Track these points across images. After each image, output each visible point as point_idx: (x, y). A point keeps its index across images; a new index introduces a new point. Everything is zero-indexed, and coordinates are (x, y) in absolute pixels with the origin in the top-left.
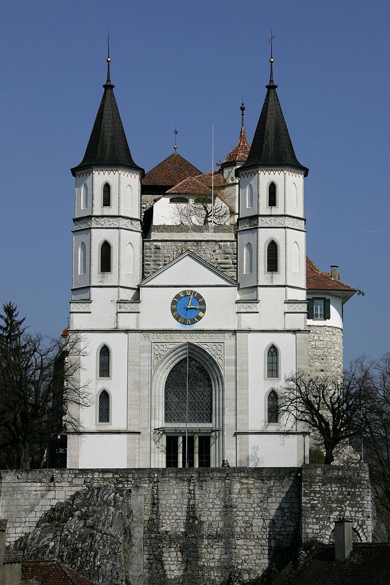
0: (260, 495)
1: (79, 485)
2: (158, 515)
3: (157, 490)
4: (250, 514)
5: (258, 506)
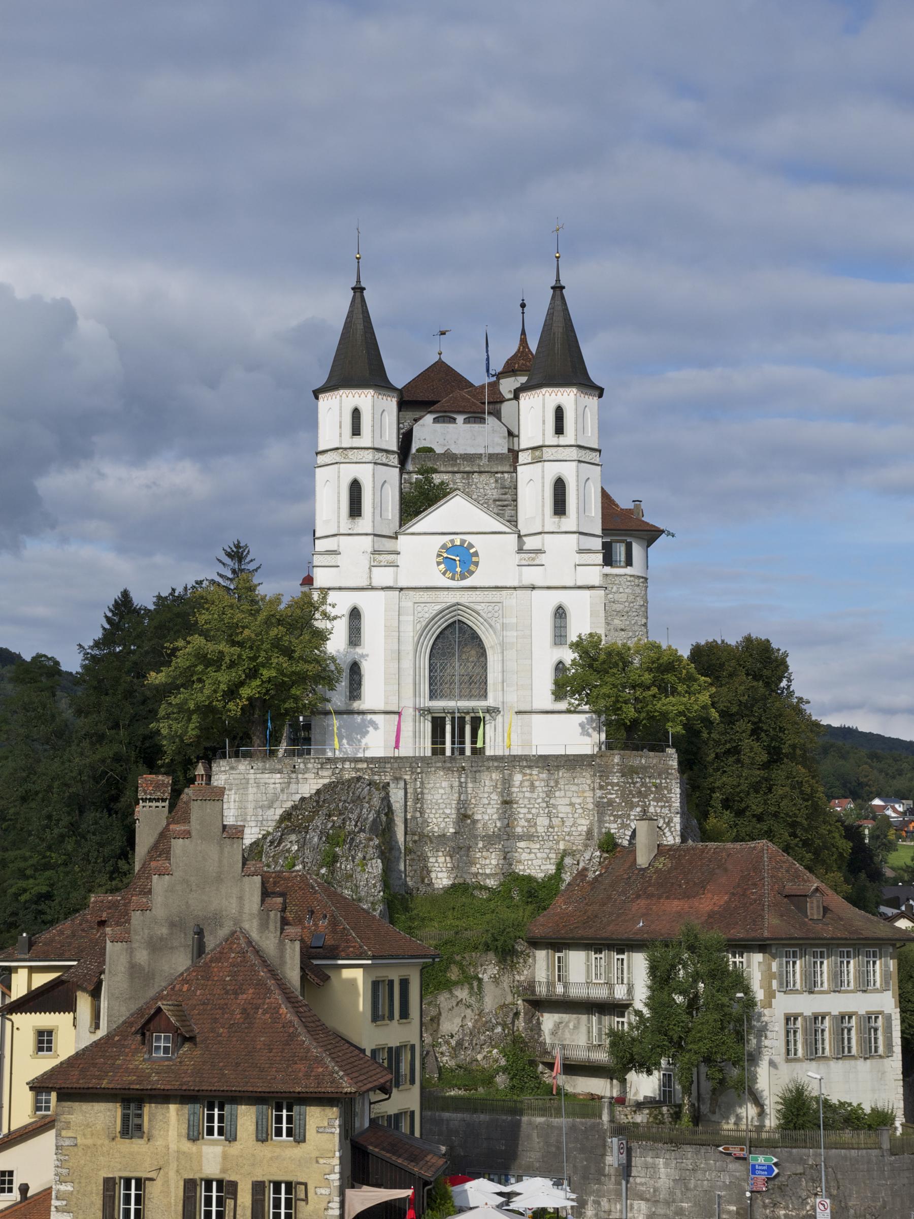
0: (546, 789)
3: (422, 783)
5: (544, 801)
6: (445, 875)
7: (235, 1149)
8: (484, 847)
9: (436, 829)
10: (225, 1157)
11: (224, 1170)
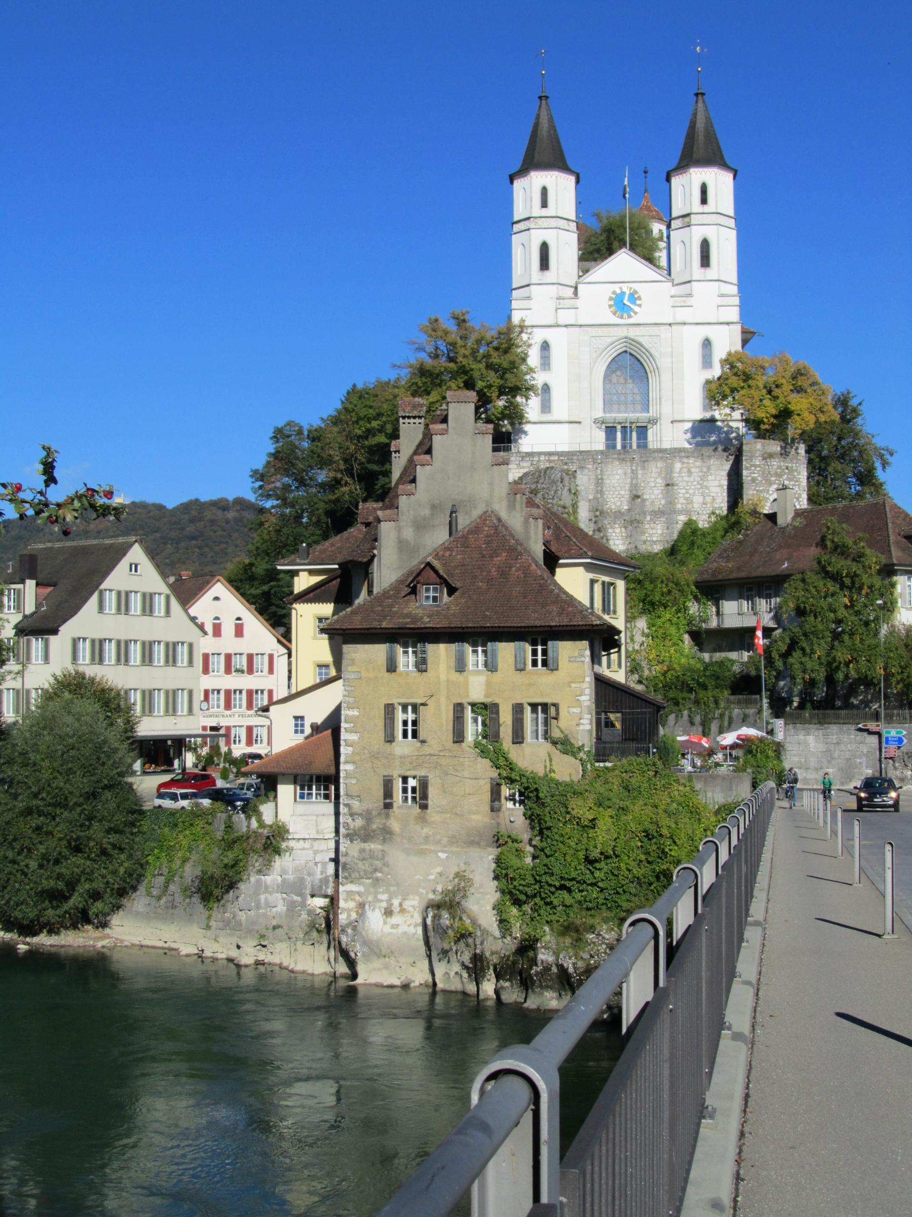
0: (700, 474)
1: (526, 467)
2: (601, 492)
3: (601, 471)
4: (691, 491)
5: (699, 484)
6: (621, 542)
7: (497, 677)
8: (651, 519)
9: (613, 507)
10: (488, 684)
11: (487, 696)
